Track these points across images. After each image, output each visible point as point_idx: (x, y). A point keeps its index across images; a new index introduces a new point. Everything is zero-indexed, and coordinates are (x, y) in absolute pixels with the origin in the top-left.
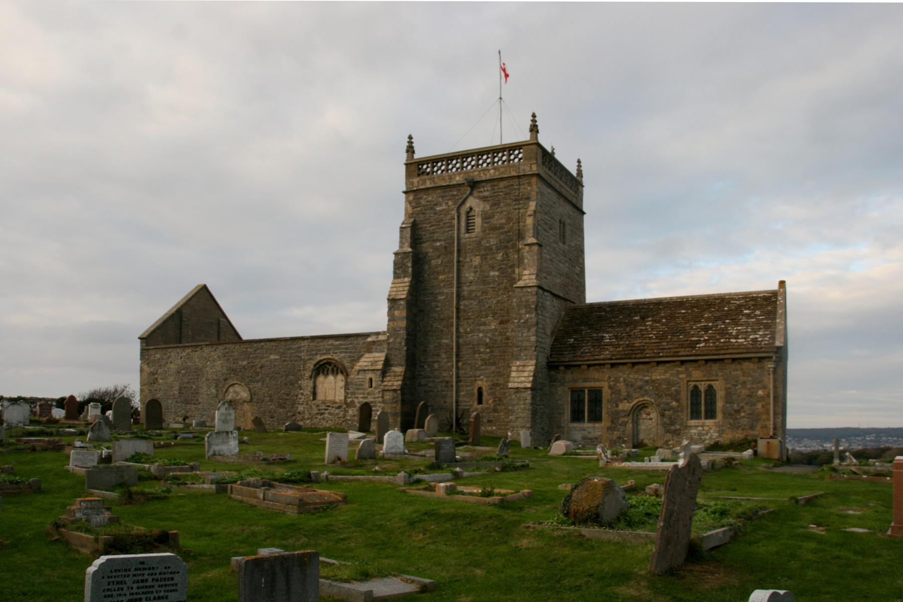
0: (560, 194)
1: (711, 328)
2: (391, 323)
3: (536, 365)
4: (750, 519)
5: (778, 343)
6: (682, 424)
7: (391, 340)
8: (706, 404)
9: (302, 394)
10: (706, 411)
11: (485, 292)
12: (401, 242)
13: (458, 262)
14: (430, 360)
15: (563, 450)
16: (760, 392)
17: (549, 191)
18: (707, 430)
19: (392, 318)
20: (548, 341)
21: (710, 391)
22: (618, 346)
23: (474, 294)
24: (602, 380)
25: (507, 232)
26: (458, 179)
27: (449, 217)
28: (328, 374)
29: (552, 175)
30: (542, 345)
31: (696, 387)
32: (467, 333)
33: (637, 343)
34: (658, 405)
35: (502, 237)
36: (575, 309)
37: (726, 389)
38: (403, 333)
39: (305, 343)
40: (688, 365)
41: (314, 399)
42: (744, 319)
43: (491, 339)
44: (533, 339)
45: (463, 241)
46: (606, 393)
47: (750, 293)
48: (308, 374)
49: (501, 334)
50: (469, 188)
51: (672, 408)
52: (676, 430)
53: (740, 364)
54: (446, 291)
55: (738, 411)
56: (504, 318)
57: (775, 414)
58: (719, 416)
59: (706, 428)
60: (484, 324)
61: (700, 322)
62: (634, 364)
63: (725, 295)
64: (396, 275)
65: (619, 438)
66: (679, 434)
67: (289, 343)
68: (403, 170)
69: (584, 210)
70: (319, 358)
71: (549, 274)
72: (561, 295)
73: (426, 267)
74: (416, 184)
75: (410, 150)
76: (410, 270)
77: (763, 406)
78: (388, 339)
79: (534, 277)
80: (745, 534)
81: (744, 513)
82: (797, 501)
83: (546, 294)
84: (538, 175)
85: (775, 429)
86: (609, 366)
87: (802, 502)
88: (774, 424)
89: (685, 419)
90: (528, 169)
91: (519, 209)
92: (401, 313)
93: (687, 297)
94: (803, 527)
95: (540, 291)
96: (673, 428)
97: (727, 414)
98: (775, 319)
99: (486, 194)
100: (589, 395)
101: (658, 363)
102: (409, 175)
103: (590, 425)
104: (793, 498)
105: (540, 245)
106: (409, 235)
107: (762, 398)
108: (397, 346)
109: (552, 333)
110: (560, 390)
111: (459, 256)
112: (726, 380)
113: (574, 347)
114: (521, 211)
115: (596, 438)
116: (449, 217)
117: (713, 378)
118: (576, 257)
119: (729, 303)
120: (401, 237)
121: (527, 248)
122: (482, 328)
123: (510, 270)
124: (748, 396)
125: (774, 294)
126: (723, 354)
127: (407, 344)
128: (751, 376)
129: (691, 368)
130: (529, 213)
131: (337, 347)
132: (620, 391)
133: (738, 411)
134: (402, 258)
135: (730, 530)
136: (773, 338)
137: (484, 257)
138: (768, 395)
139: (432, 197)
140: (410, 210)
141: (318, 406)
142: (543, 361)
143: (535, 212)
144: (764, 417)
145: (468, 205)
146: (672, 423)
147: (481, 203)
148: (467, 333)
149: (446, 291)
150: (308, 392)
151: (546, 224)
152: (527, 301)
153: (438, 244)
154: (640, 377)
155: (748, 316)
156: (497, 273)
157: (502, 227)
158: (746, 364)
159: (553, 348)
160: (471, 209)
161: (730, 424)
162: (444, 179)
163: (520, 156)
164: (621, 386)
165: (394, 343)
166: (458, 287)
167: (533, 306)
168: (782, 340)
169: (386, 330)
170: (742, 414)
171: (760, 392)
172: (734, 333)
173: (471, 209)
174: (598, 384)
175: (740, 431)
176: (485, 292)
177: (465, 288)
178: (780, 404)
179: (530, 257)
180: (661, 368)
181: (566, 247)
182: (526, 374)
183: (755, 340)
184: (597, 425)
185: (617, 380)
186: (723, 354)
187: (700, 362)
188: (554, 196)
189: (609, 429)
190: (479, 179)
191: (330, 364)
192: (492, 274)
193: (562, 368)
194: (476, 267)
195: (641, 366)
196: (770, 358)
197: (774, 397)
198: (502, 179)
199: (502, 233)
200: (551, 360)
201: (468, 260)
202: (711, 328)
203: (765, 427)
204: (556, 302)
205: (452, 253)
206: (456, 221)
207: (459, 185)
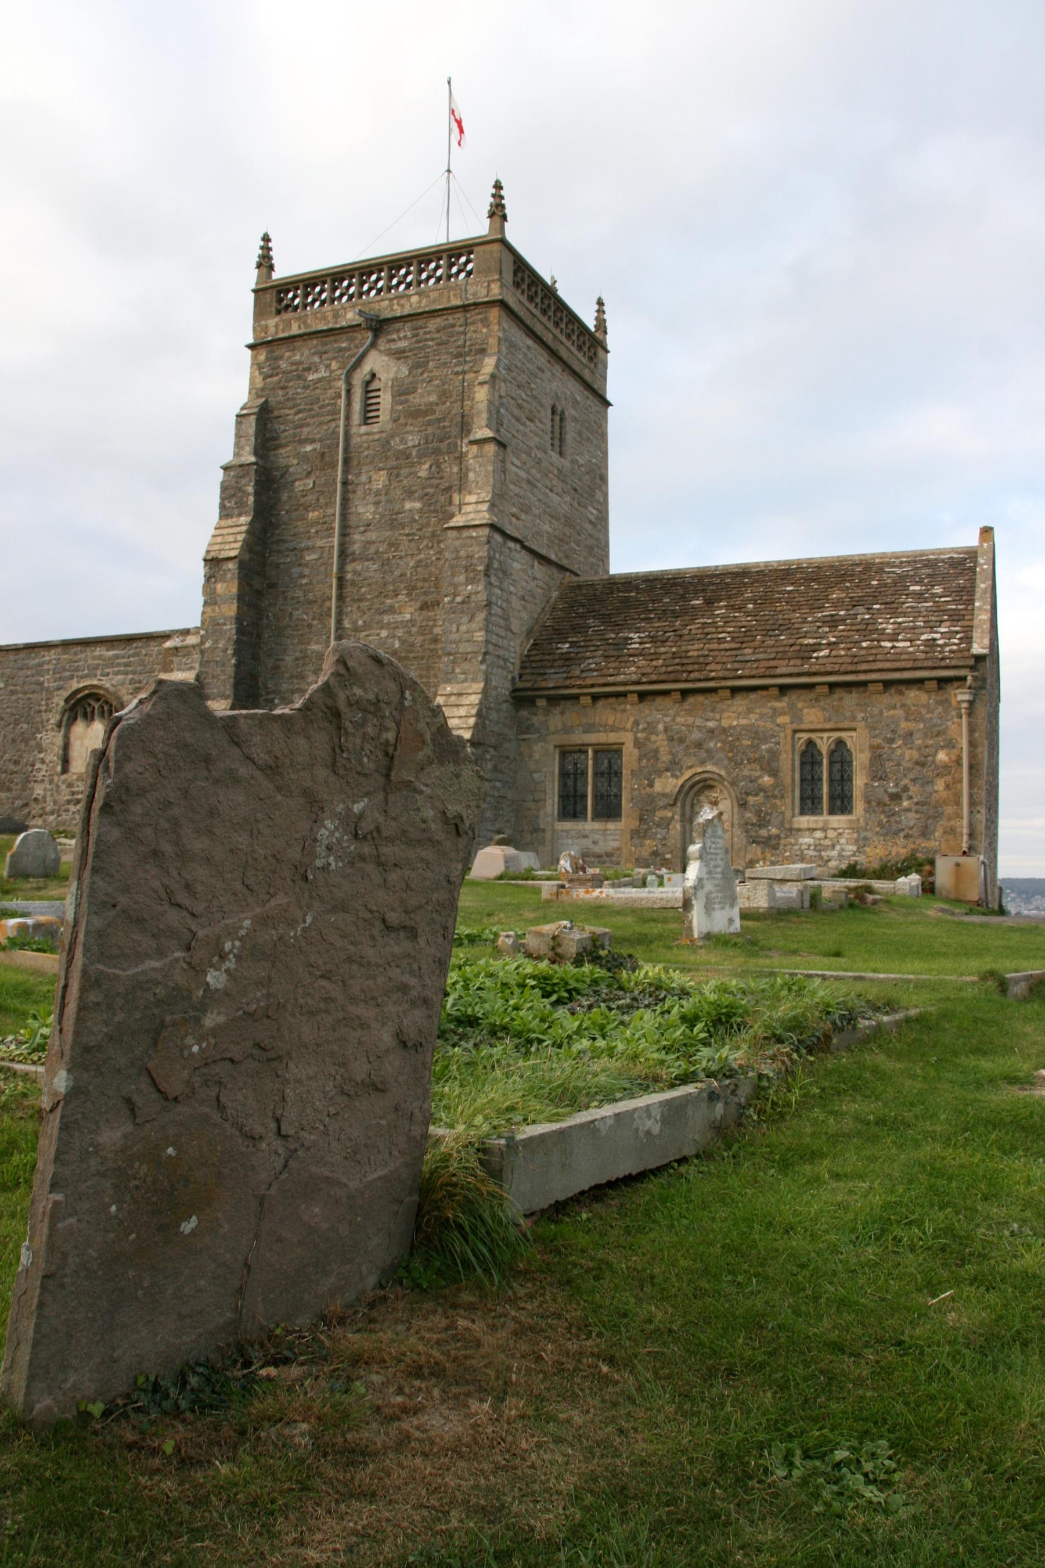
0: (553, 354)
1: (843, 621)
2: (209, 609)
3: (485, 692)
4: (820, 1045)
5: (978, 648)
6: (782, 823)
7: (207, 645)
8: (831, 781)
9: (43, 761)
10: (832, 798)
11: (393, 545)
12: (237, 445)
13: (345, 483)
14: (285, 686)
15: (499, 868)
16: (942, 756)
17: (530, 342)
18: (831, 839)
19: (211, 599)
20: (516, 648)
21: (841, 754)
22: (656, 656)
23: (372, 550)
24: (621, 727)
25: (439, 420)
26: (351, 317)
27: (331, 392)
28: (93, 719)
29: (537, 312)
30: (501, 653)
31: (810, 743)
32: (357, 629)
33: (694, 650)
34: (733, 784)
35: (430, 430)
36: (579, 587)
37: (872, 747)
38: (230, 628)
39: (51, 655)
40: (794, 695)
41: (65, 770)
42: (910, 603)
43: (403, 642)
44: (480, 636)
45: (355, 441)
46: (630, 756)
47: (923, 553)
48: (54, 718)
49: (422, 631)
50: (370, 335)
51: (762, 789)
52: (770, 838)
53: (901, 693)
54: (320, 543)
55: (896, 797)
56: (430, 598)
57: (972, 804)
58: (859, 806)
59: (831, 834)
60: (391, 610)
61: (821, 608)
62: (685, 693)
63: (874, 556)
64: (225, 512)
65: (655, 854)
66: (775, 847)
67: (22, 655)
68: (249, 300)
69: (610, 396)
70: (75, 685)
71: (526, 509)
72: (553, 557)
73: (285, 496)
74: (272, 330)
75: (265, 263)
76: (252, 499)
77: (947, 787)
78: (202, 643)
79: (485, 507)
80: (778, 1115)
81: (795, 1025)
82: (1003, 986)
83: (511, 544)
84: (502, 304)
85: (971, 835)
86: (635, 697)
87: (1019, 989)
88: (971, 825)
89: (788, 814)
90: (484, 292)
91: (464, 372)
92: (228, 587)
93: (799, 562)
94: (1012, 1080)
95: (498, 538)
96: (763, 832)
97: (873, 803)
98: (972, 602)
99: (403, 344)
100: (595, 759)
101: (735, 691)
102: (260, 312)
103: (597, 825)
104: (992, 974)
105: (502, 445)
106: (252, 431)
107: (945, 770)
108: (218, 656)
109: (529, 633)
110: (538, 748)
111: (346, 471)
112: (872, 728)
113: (568, 660)
114: (467, 377)
115: (609, 855)
116: (331, 392)
117: (846, 724)
118: (593, 485)
119: (880, 571)
120: (238, 436)
121: (475, 448)
122: (386, 618)
123: (442, 499)
124: (917, 763)
125: (972, 554)
126: (865, 672)
127: (237, 652)
128: (922, 719)
129: (799, 700)
130: (481, 378)
131: (110, 663)
132: (656, 751)
133: (896, 797)
134: (237, 477)
135: (712, 1096)
136: (968, 639)
137: (394, 473)
138: (958, 762)
139: (302, 354)
140: (259, 382)
141: (70, 785)
142: (504, 688)
143: (493, 376)
144: (949, 810)
145: (367, 368)
146: (763, 822)
147: (392, 363)
148: (357, 629)
149: (320, 543)
150: (53, 757)
151: (520, 407)
152: (469, 557)
153: (309, 448)
154: (699, 722)
155: (919, 596)
156: (418, 505)
157: (429, 410)
158: (913, 695)
159: (526, 663)
160: (373, 376)
161: (881, 825)
162: (325, 318)
163: (470, 267)
164: (660, 741)
165: (213, 649)
166: (344, 535)
167: (481, 568)
168: (986, 642)
169: (199, 625)
170: (905, 804)
171: (942, 756)
172: (890, 629)
173: (373, 376)
174: (612, 737)
175: (901, 841)
176: (393, 545)
177: (356, 537)
178: (982, 782)
179: (480, 465)
180: (740, 703)
181: (566, 463)
182: (462, 712)
183: (931, 643)
184: (611, 826)
185: (651, 728)
186: (865, 672)
187: (819, 689)
188: (541, 358)
189: (635, 834)
190: (388, 315)
191: (97, 697)
192: (408, 505)
193: (541, 703)
194: (378, 493)
195: (700, 698)
196: (964, 679)
197: (971, 767)
198: (432, 314)
199: (429, 423)
200: (520, 685)
201: (364, 478)
202: (843, 621)
203: (951, 831)
204: (539, 570)
205: (333, 466)
206: (342, 402)
207: (353, 328)
